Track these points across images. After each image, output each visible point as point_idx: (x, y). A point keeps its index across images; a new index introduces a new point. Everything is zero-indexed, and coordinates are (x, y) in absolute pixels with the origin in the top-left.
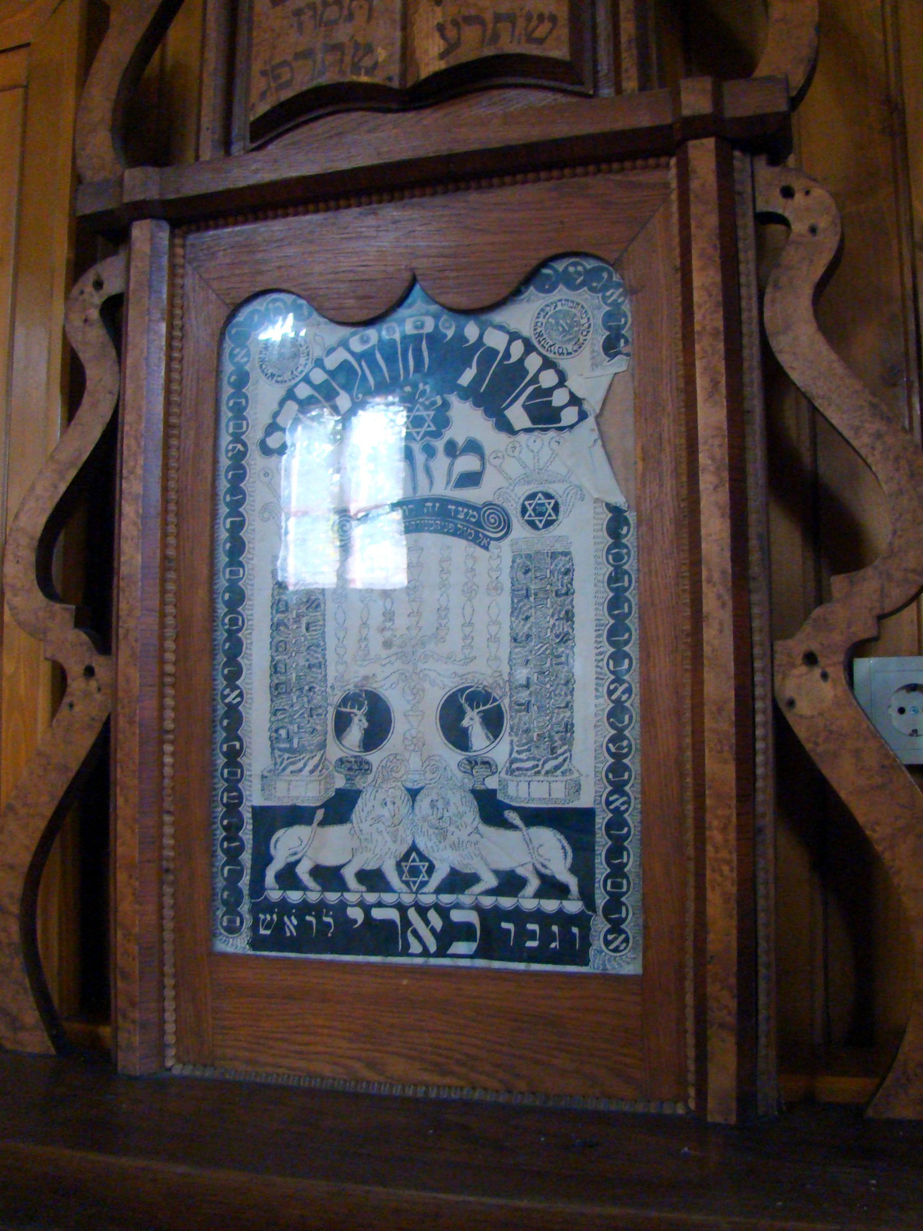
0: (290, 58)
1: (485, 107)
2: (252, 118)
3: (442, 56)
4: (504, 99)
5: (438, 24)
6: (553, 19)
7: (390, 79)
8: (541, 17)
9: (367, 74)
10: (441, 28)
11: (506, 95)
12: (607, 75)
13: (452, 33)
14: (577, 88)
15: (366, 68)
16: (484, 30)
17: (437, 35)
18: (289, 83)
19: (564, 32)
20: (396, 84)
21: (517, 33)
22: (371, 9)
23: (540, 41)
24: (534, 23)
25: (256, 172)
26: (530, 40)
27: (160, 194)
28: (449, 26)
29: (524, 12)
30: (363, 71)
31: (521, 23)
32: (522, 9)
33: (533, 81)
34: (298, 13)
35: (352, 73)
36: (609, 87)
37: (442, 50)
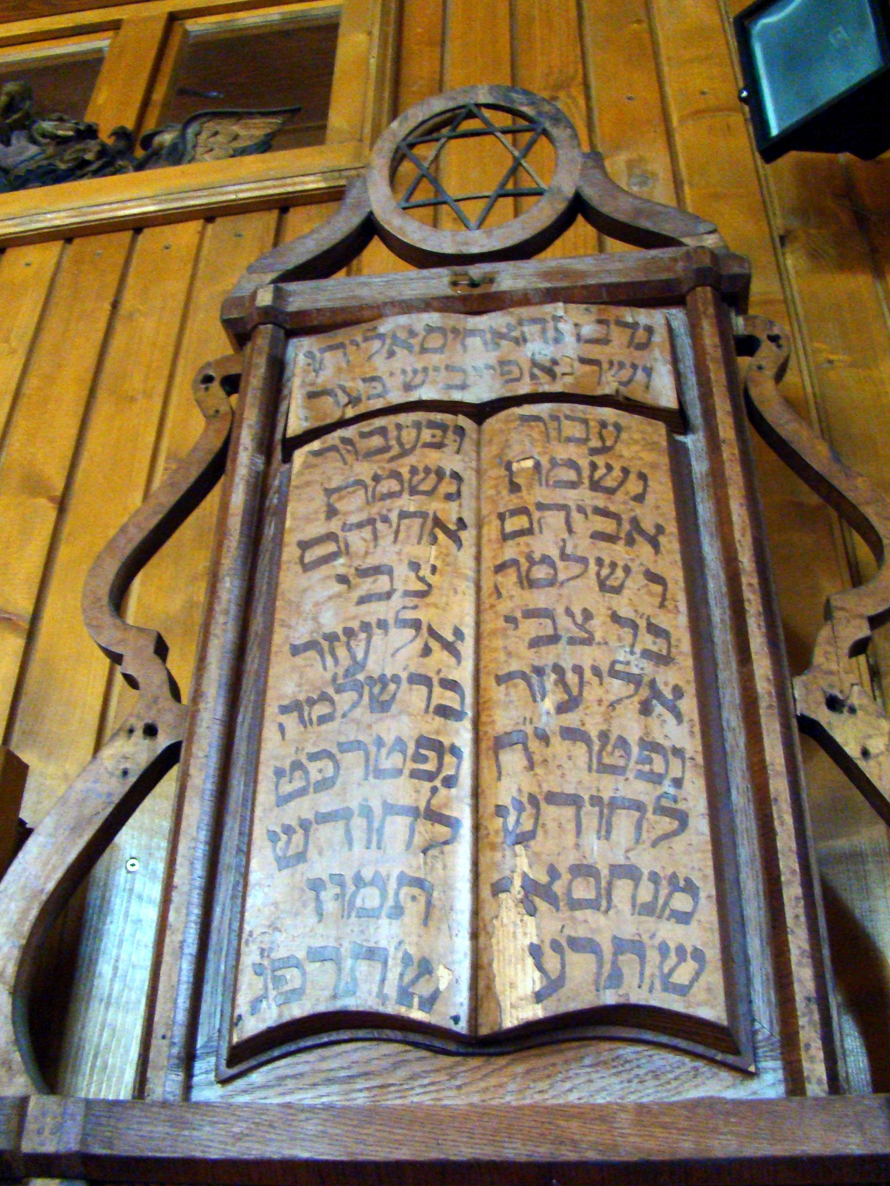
0: (301, 955)
1: (590, 1066)
2: (235, 1040)
3: (539, 997)
4: (618, 1057)
5: (532, 944)
6: (698, 955)
7: (456, 1019)
8: (681, 951)
9: (421, 1007)
10: (535, 951)
11: (621, 1052)
12: (768, 1039)
13: (552, 962)
14: (730, 1059)
15: (420, 997)
16: (600, 964)
17: (530, 961)
18: (298, 993)
19: (714, 977)
20: (462, 1027)
21: (648, 972)
22: (429, 904)
23: (682, 990)
24: (673, 959)
25: (238, 1138)
26: (669, 987)
27: (83, 1142)
28: (547, 950)
29: (657, 941)
30: (416, 1000)
31: (653, 956)
32: (653, 936)
33: (664, 1039)
34: (316, 886)
35: (400, 1002)
36: (774, 1059)
37: (537, 988)
